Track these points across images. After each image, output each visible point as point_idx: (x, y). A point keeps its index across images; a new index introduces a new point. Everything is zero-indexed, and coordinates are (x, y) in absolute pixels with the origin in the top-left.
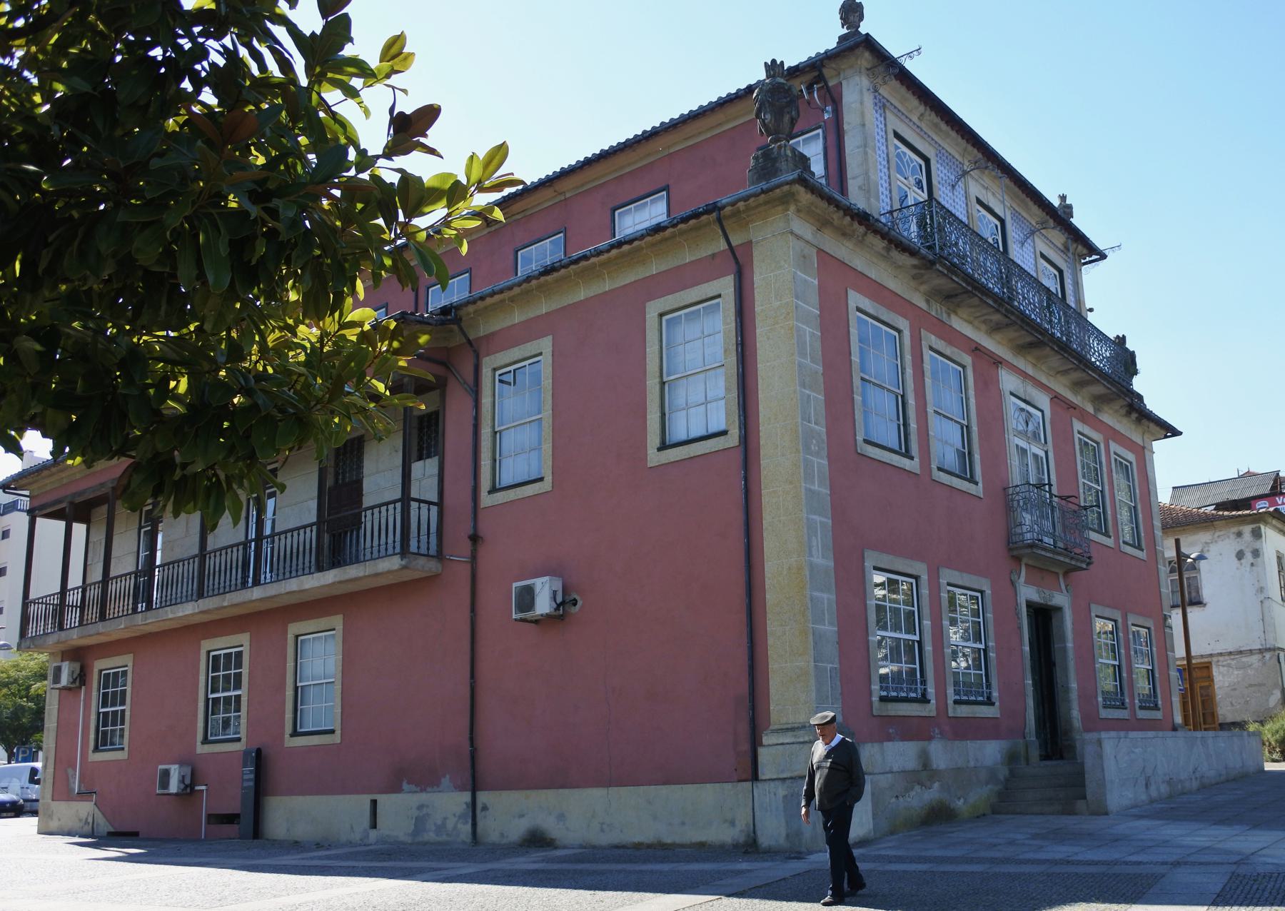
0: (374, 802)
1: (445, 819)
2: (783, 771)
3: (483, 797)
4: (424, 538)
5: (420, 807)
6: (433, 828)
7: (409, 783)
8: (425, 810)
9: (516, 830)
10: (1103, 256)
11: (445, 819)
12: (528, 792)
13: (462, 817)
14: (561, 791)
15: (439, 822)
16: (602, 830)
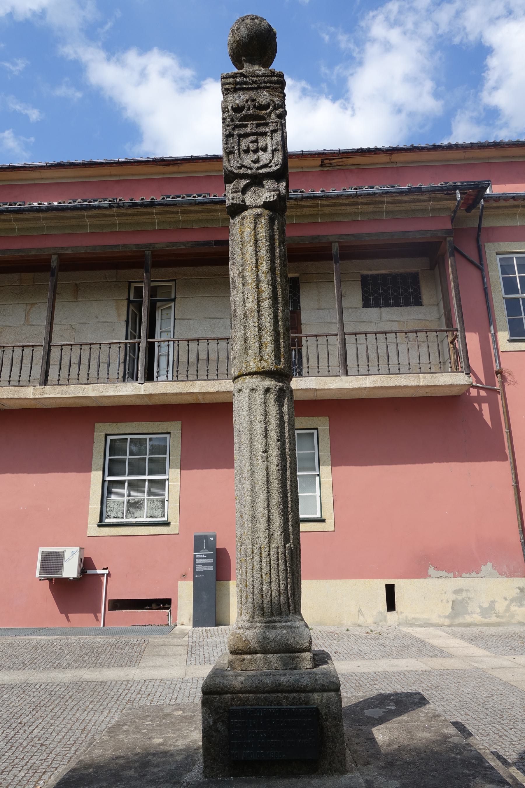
1: (493, 602)
5: (456, 592)
7: (437, 569)
8: (464, 595)
11: (493, 602)
15: (486, 605)
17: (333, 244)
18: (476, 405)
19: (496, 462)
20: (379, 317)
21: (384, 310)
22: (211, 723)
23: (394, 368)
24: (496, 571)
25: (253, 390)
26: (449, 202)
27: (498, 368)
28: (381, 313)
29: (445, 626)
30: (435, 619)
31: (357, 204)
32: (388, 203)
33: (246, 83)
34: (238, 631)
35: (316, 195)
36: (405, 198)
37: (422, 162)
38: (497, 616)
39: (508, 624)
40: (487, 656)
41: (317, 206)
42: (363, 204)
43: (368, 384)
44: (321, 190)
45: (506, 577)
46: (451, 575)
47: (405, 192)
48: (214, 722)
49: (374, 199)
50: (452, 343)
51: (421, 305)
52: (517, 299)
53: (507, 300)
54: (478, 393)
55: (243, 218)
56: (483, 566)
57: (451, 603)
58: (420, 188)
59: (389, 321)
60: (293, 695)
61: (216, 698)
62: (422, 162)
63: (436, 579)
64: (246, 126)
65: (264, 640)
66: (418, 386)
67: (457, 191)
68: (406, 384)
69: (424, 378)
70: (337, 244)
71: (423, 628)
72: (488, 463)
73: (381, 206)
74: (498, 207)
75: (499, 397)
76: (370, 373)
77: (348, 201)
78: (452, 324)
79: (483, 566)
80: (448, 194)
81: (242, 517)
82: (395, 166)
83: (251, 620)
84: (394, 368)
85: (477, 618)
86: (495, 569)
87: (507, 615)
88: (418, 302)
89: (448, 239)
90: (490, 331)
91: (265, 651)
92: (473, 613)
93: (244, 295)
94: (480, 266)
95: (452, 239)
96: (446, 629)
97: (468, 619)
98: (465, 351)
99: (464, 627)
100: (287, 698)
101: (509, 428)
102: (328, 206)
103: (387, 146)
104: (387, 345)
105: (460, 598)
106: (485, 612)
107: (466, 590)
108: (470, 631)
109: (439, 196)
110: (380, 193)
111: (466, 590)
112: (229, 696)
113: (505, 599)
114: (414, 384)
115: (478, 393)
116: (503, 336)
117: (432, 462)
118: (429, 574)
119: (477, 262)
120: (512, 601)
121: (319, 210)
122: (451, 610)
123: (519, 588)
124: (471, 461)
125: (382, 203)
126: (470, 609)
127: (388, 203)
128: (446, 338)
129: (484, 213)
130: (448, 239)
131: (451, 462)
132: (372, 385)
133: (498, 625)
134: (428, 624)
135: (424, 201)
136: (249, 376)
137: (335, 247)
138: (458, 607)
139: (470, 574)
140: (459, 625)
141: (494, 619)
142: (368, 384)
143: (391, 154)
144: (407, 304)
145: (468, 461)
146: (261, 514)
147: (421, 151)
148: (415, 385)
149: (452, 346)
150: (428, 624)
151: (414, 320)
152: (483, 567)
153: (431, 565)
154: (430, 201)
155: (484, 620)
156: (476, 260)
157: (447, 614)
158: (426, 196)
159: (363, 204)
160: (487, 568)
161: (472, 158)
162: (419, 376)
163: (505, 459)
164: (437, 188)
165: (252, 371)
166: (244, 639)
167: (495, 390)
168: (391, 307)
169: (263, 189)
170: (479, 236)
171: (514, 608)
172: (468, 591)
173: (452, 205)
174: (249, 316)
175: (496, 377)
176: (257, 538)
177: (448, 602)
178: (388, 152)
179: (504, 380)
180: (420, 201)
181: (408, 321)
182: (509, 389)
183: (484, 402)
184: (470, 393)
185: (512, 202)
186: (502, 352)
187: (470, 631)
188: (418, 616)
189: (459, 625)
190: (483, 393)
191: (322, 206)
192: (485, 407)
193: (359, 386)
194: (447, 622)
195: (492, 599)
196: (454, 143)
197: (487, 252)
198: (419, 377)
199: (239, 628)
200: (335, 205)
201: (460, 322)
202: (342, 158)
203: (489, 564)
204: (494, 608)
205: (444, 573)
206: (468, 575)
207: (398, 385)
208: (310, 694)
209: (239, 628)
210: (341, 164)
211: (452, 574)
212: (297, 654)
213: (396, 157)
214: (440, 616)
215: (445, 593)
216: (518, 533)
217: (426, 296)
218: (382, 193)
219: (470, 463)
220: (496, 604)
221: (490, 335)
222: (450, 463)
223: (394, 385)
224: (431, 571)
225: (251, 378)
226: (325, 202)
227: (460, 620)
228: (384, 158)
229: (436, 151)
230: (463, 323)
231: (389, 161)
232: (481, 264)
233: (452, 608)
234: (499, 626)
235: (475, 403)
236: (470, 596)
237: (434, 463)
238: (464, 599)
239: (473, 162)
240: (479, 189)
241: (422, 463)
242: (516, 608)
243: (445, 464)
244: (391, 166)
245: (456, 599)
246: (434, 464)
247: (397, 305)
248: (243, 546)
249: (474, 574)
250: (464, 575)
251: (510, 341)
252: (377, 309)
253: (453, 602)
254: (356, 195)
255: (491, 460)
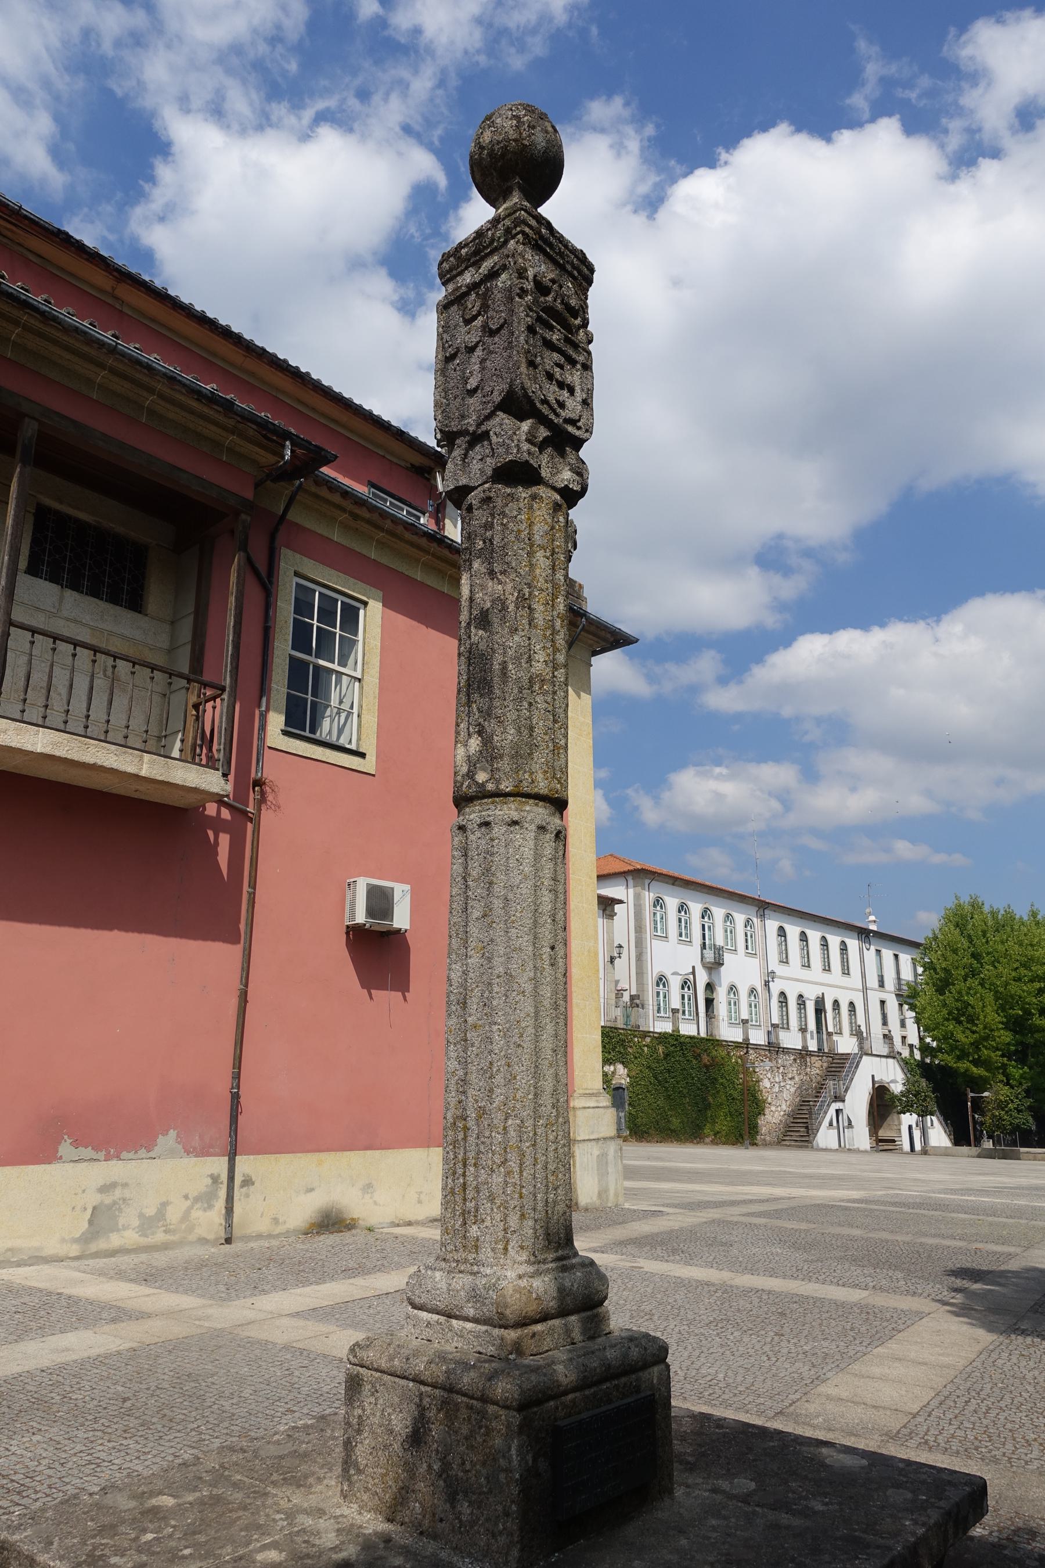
0: (843, 943)
1: (164, 1205)
2: (592, 1132)
3: (244, 1164)
4: (39, 678)
5: (104, 1189)
6: (136, 1223)
7: (76, 1144)
8: (118, 1193)
9: (301, 1210)
10: (637, 640)
11: (164, 1205)
12: (323, 1156)
13: (206, 1199)
14: (369, 1152)
15: (151, 1211)
16: (420, 1202)
17: (27, 420)
18: (211, 833)
19: (221, 943)
20: (57, 605)
21: (70, 595)
22: (530, 1462)
23: (56, 717)
24: (180, 1147)
25: (542, 828)
26: (262, 452)
27: (260, 774)
28: (61, 599)
29: (70, 1258)
30: (52, 1247)
31: (102, 366)
32: (161, 396)
33: (551, 245)
34: (523, 1283)
35: (31, 301)
36: (194, 404)
37: (170, 329)
38: (165, 1232)
39: (181, 1243)
40: (204, 1306)
41: (16, 323)
42: (112, 371)
43: (39, 745)
44: (44, 296)
45: (196, 1156)
46: (101, 1155)
47: (205, 396)
48: (535, 1460)
49: (138, 375)
50: (196, 707)
51: (140, 612)
52: (306, 664)
53: (291, 657)
54: (219, 812)
55: (534, 497)
56: (160, 1136)
57: (89, 1211)
58: (230, 404)
59: (75, 621)
60: (623, 1380)
61: (535, 1413)
62: (170, 329)
63: (72, 1164)
64: (551, 328)
65: (562, 1292)
66: (136, 776)
67: (288, 443)
68: (115, 766)
69: (151, 762)
70: (35, 425)
71: (27, 1269)
72: (209, 944)
73: (145, 394)
74: (316, 496)
75: (250, 826)
76: (47, 724)
77: (86, 349)
78: (202, 672)
79: (160, 1136)
80: (265, 437)
81: (509, 1066)
82: (118, 306)
83: (532, 1258)
84: (56, 717)
85: (130, 1237)
86: (179, 1143)
87: (183, 1227)
88: (135, 603)
89: (243, 516)
90: (259, 706)
91: (562, 1313)
92: (125, 1228)
93: (530, 644)
94: (266, 581)
95: (249, 519)
96: (76, 1264)
97: (115, 1240)
98: (229, 732)
99: (106, 1256)
100: (617, 1386)
101: (253, 885)
102: (40, 335)
103: (120, 262)
104: (52, 666)
105: (108, 1200)
106: (147, 1224)
107: (122, 1185)
108: (125, 1261)
109: (251, 433)
110: (160, 371)
111: (122, 1185)
112: (552, 1403)
113: (186, 1197)
114: (131, 769)
115: (219, 812)
116: (276, 721)
117: (111, 929)
118: (59, 1154)
119: (264, 574)
120: (197, 1199)
121: (16, 333)
122: (87, 1226)
123: (212, 1176)
124: (181, 937)
125: (151, 390)
126: (121, 1221)
127: (161, 396)
128: (184, 691)
129: (298, 497)
130: (243, 516)
131: (146, 932)
132: (48, 750)
133: (165, 1247)
134: (38, 1259)
135: (224, 428)
136: (531, 801)
137: (29, 430)
138: (101, 1219)
139: (136, 1152)
140: (96, 1255)
141: (160, 1237)
142: (39, 745)
143: (118, 281)
144: (114, 599)
145: (176, 936)
146: (546, 1062)
147: (174, 310)
148: (132, 771)
149: (194, 712)
150: (38, 1259)
151: (123, 637)
152: (161, 1139)
153: (66, 1137)
154: (233, 433)
155: (144, 1241)
156: (264, 574)
157: (78, 1236)
158: (230, 423)
159: (112, 371)
160: (168, 1140)
161: (252, 374)
162: (141, 757)
163: (236, 941)
164: (259, 420)
165: (541, 792)
166: (534, 1296)
167: (245, 813)
168: (82, 592)
169: (561, 460)
170: (277, 531)
171: (197, 1214)
172: (125, 1185)
173: (266, 458)
174: (536, 687)
175: (252, 787)
176: (540, 1105)
177: (85, 1209)
178: (115, 274)
179: (263, 800)
180: (217, 424)
181: (111, 633)
182: (267, 817)
183: (225, 832)
184: (205, 809)
185: (336, 498)
186: (270, 748)
187: (125, 1261)
188: (18, 1243)
189: (96, 1255)
190: (226, 814)
191: (26, 328)
192: (224, 839)
193: (19, 746)
194: (74, 1250)
195: (165, 1200)
196: (224, 324)
197: (282, 564)
198: (141, 758)
199: (520, 1277)
200: (55, 342)
201: (231, 677)
202: (16, 225)
203: (172, 1133)
204: (164, 1215)
205: (88, 1152)
206: (131, 1155)
207: (99, 763)
208: (641, 1374)
209: (520, 1277)
210: (9, 234)
211: (104, 1152)
212: (595, 1311)
213: (124, 291)
214: (63, 1240)
215: (84, 1191)
216: (230, 1075)
217: (155, 597)
218: (165, 374)
219: (178, 940)
220: (169, 1208)
221: (257, 712)
222: (143, 935)
223: (92, 761)
224: (65, 1148)
225: (537, 805)
226: (37, 323)
227: (102, 1245)
228: (101, 279)
229: (200, 325)
230: (236, 680)
231: (109, 289)
232: (271, 582)
233: (91, 1222)
234: (166, 1249)
235: (210, 829)
236: (128, 1196)
237: (116, 931)
238: (115, 1203)
239: (251, 380)
240: (313, 457)
241: (92, 928)
242: (200, 1213)
243: (136, 935)
244: (110, 301)
245: (102, 1203)
246: (116, 933)
247: (95, 593)
248: (510, 1122)
249: (142, 1153)
250: (124, 1155)
251: (285, 733)
252: (54, 588)
253: (94, 1208)
254: (113, 350)
255: (214, 940)
